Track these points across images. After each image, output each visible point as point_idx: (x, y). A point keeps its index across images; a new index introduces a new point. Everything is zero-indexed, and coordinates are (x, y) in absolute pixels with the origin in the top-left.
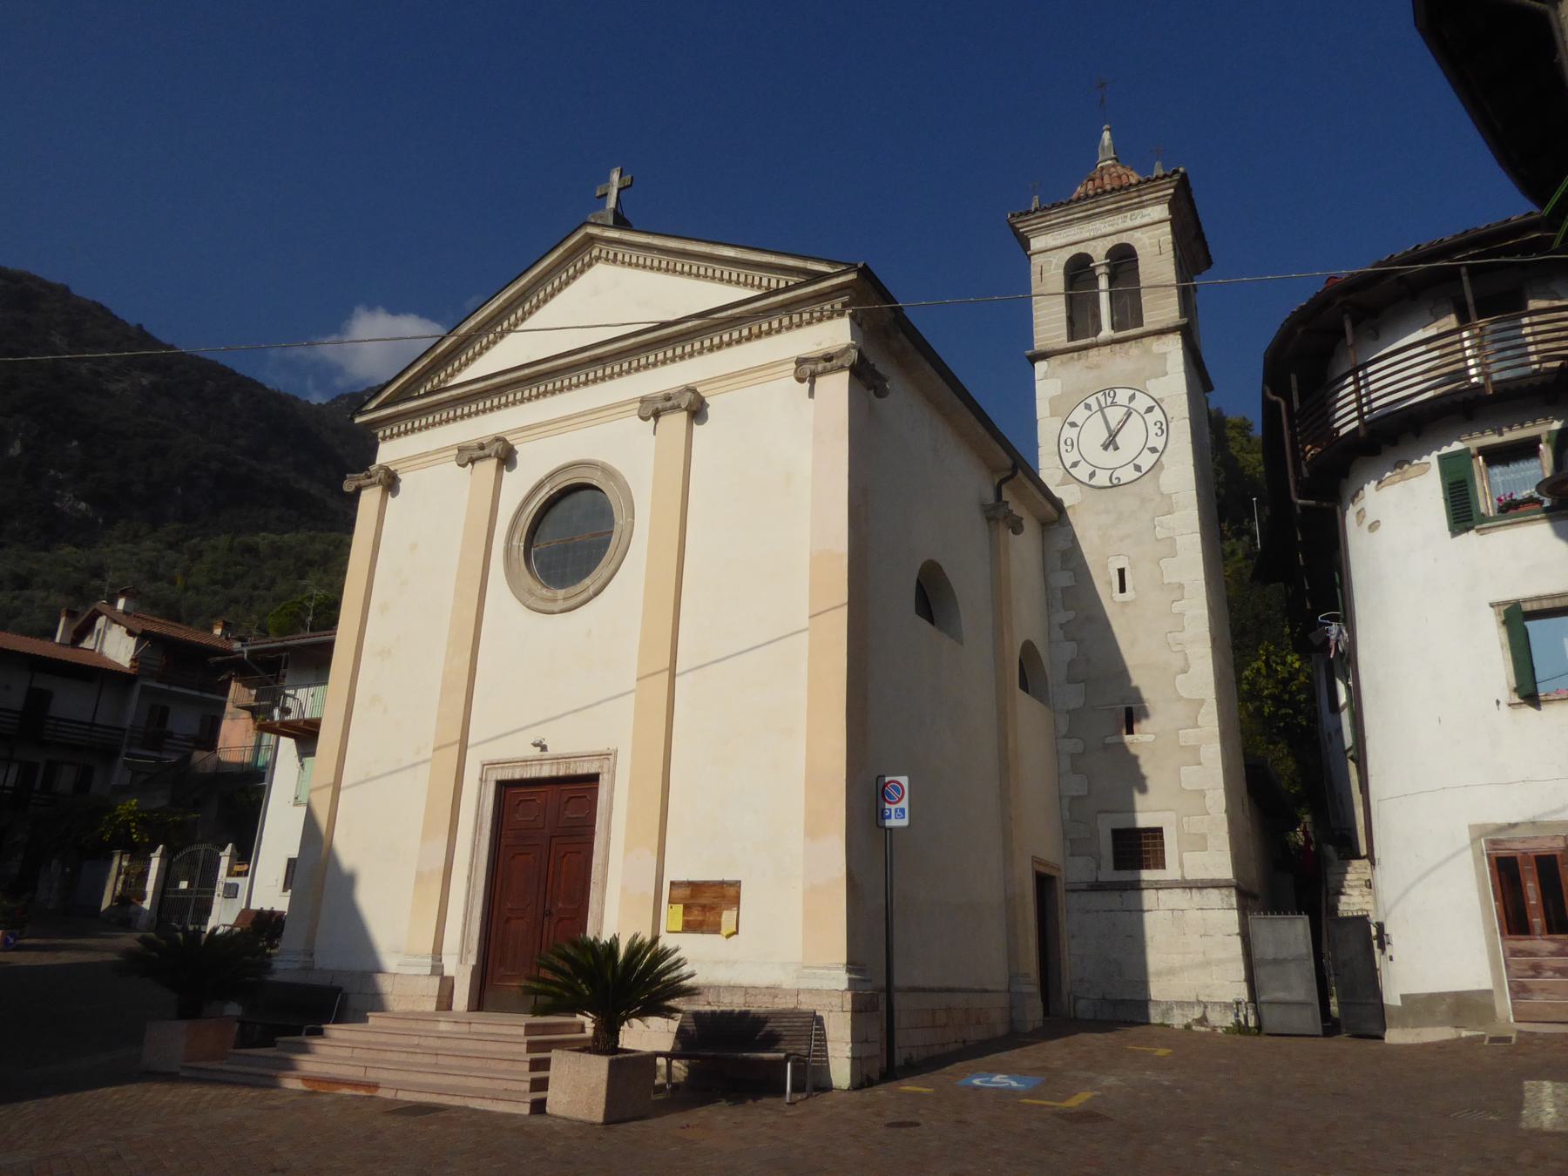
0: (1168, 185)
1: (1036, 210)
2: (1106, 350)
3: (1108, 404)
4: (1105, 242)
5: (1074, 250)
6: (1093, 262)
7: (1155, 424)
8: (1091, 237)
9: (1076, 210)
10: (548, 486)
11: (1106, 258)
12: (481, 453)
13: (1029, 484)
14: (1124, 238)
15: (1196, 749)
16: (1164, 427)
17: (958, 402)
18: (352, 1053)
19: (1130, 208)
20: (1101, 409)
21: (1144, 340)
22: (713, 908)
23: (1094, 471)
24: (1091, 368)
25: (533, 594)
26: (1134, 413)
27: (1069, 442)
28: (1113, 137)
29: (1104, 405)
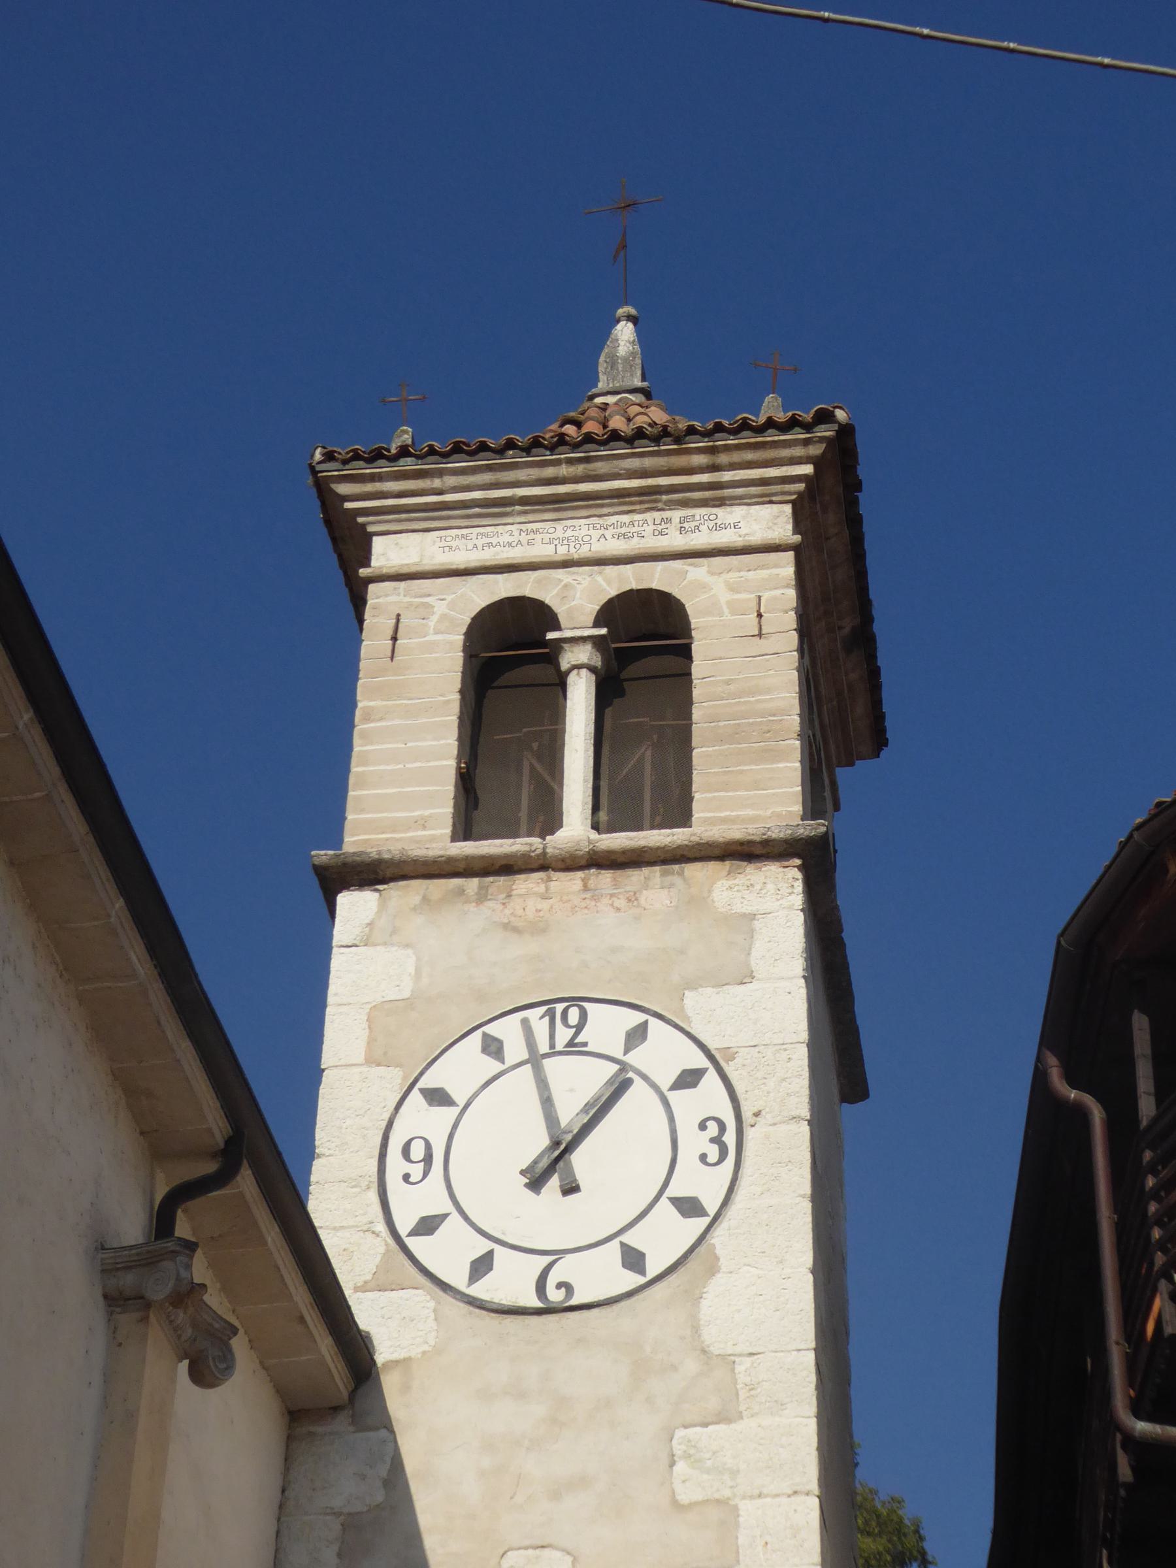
0: (798, 451)
1: (404, 452)
2: (572, 882)
3: (559, 1046)
4: (599, 579)
6: (557, 627)
7: (703, 1126)
8: (557, 558)
9: (521, 475)
11: (597, 624)
13: (272, 1235)
14: (656, 577)
16: (730, 1138)
17: (76, 825)
19: (683, 498)
20: (535, 1060)
21: (692, 870)
23: (490, 1254)
24: (516, 930)
26: (638, 1081)
27: (418, 1151)
28: (643, 338)
29: (544, 1048)
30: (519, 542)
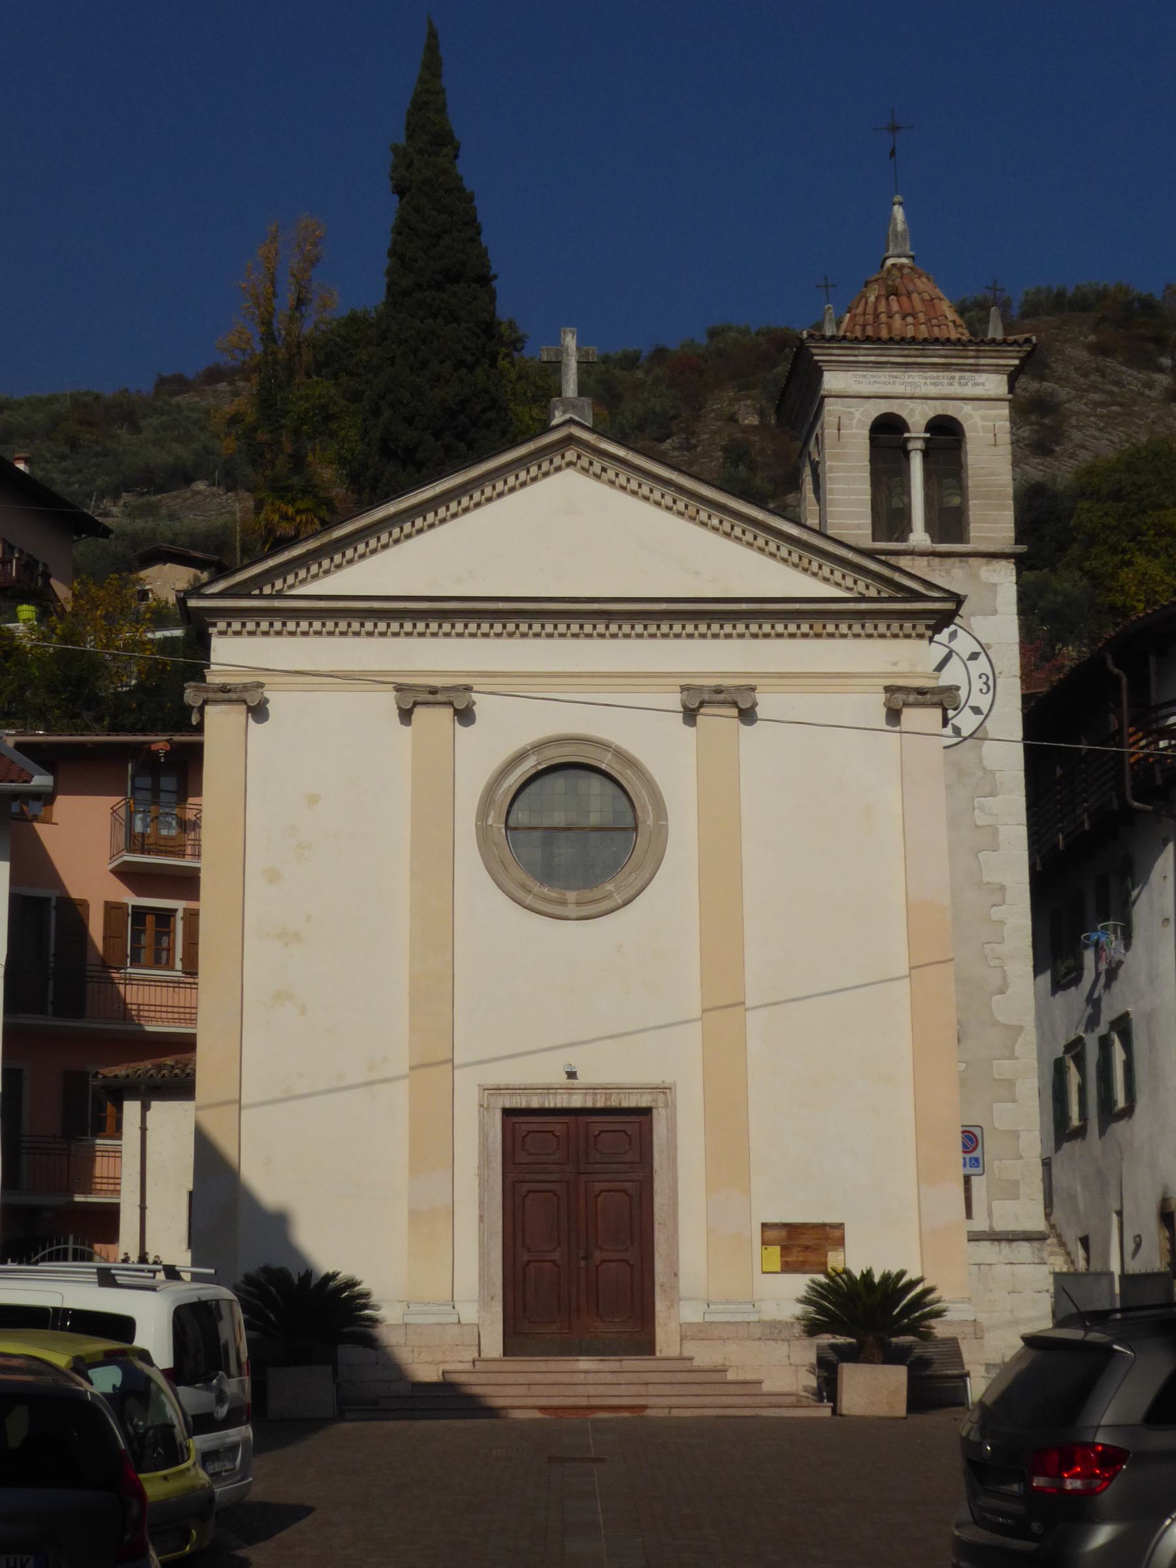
5: (885, 407)
6: (908, 431)
7: (980, 677)
9: (893, 352)
10: (535, 758)
11: (926, 431)
12: (430, 698)
14: (950, 409)
15: (1010, 1083)
16: (991, 683)
18: (529, 1390)
22: (816, 1249)
25: (530, 892)
30: (889, 383)
